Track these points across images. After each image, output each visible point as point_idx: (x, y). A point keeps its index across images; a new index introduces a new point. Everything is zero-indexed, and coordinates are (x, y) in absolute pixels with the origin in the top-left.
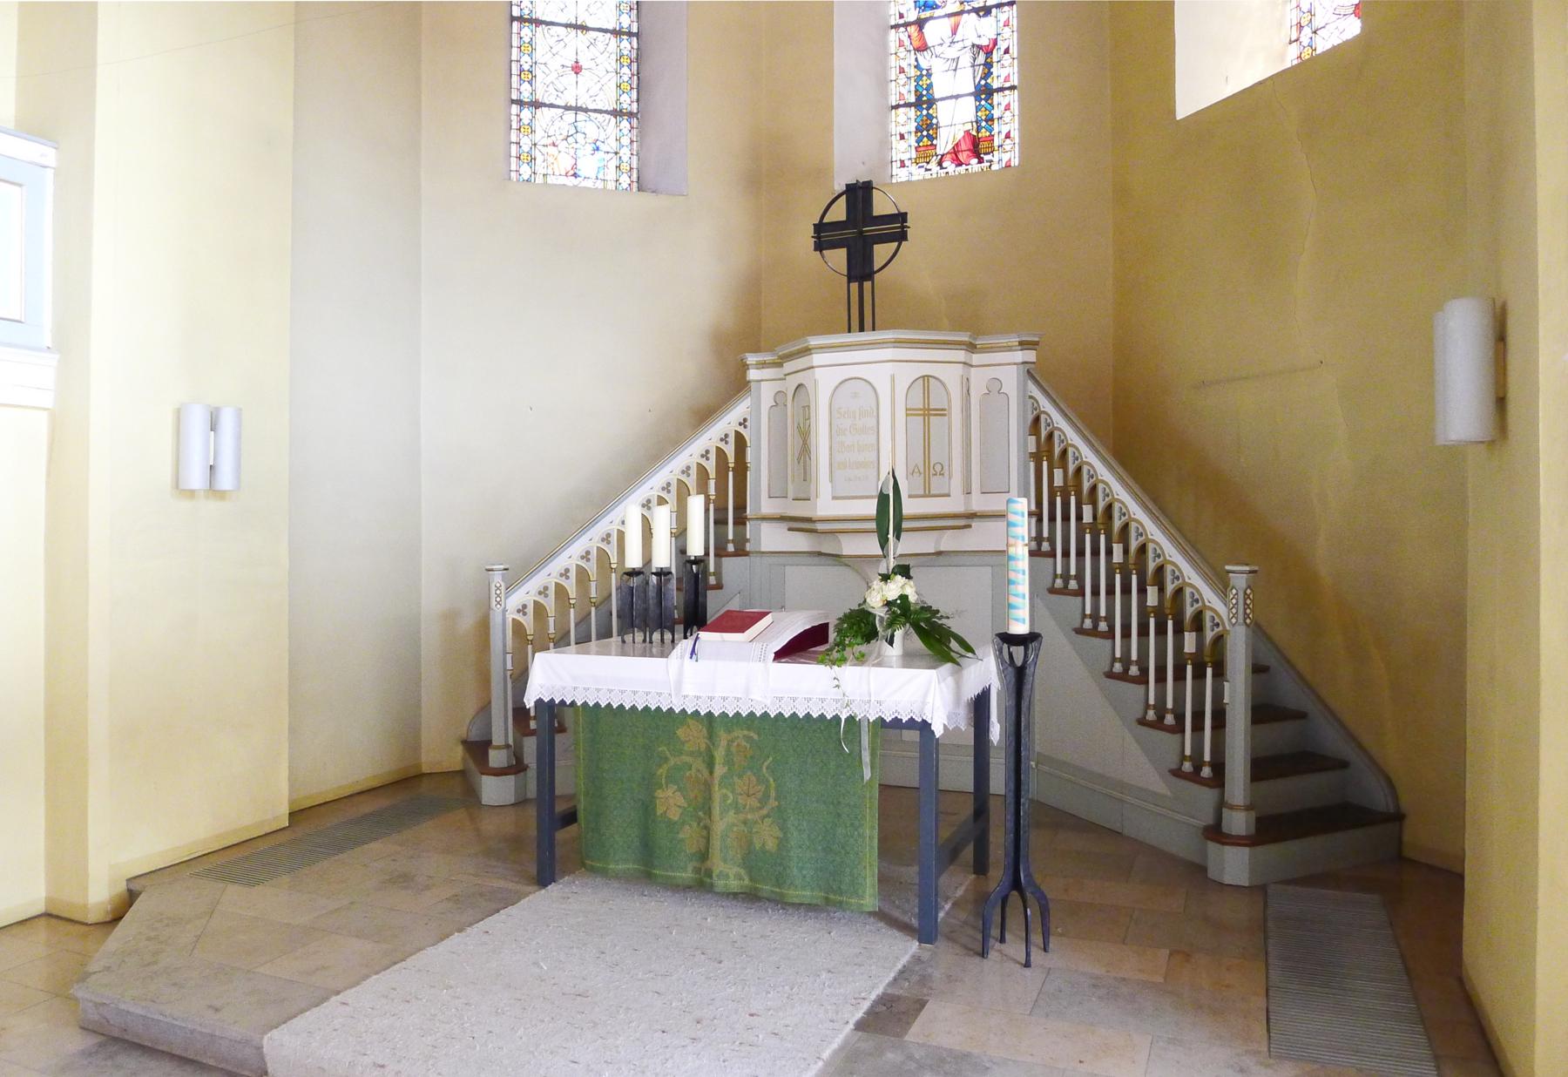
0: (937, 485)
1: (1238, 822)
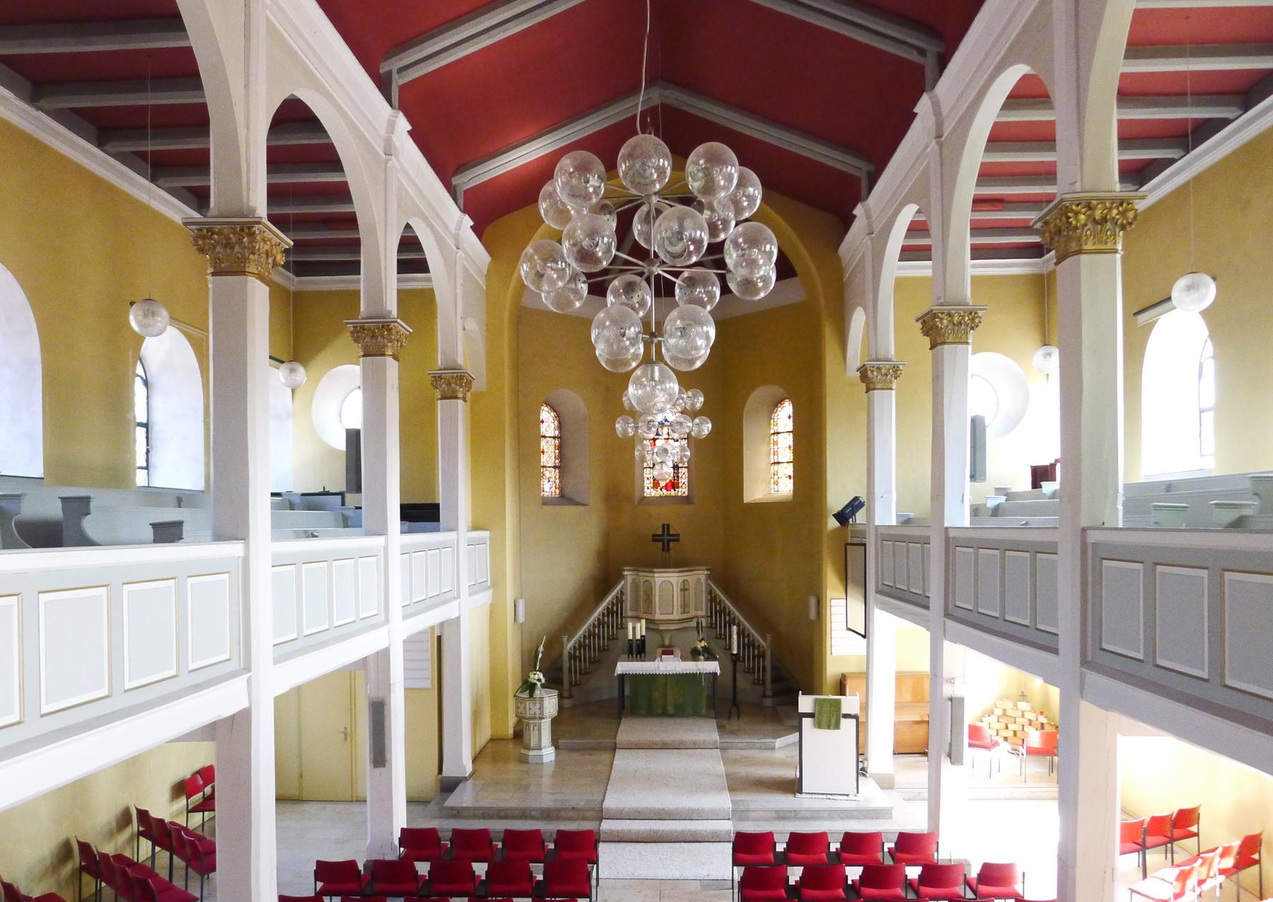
0: (687, 610)
1: (769, 693)
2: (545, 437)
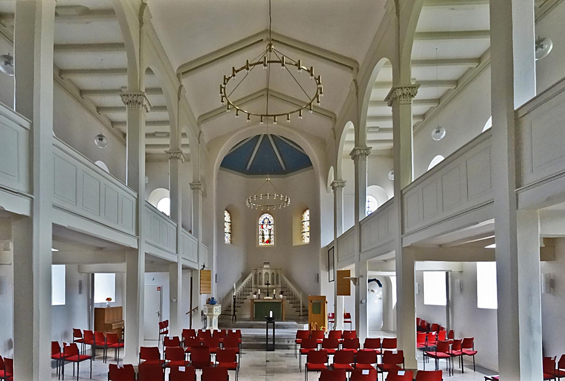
2: (226, 222)
